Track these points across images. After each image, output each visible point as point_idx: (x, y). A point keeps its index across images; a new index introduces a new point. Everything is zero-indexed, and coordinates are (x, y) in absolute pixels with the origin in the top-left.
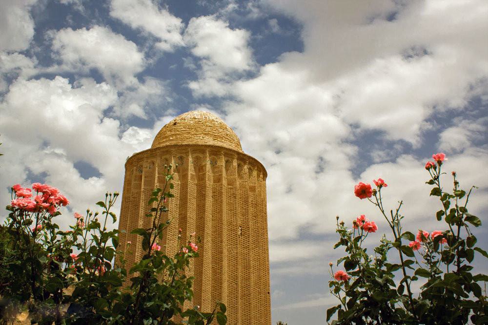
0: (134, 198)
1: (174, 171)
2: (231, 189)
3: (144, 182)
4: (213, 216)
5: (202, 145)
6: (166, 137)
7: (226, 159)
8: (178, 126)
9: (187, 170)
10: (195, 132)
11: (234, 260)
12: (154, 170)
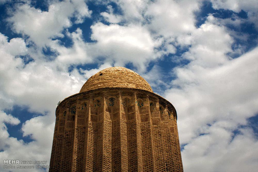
0: (67, 135)
1: (107, 110)
2: (156, 128)
3: (78, 121)
4: (143, 151)
5: (130, 89)
7: (151, 102)
8: (104, 76)
9: (119, 109)
10: (120, 80)
12: (87, 110)
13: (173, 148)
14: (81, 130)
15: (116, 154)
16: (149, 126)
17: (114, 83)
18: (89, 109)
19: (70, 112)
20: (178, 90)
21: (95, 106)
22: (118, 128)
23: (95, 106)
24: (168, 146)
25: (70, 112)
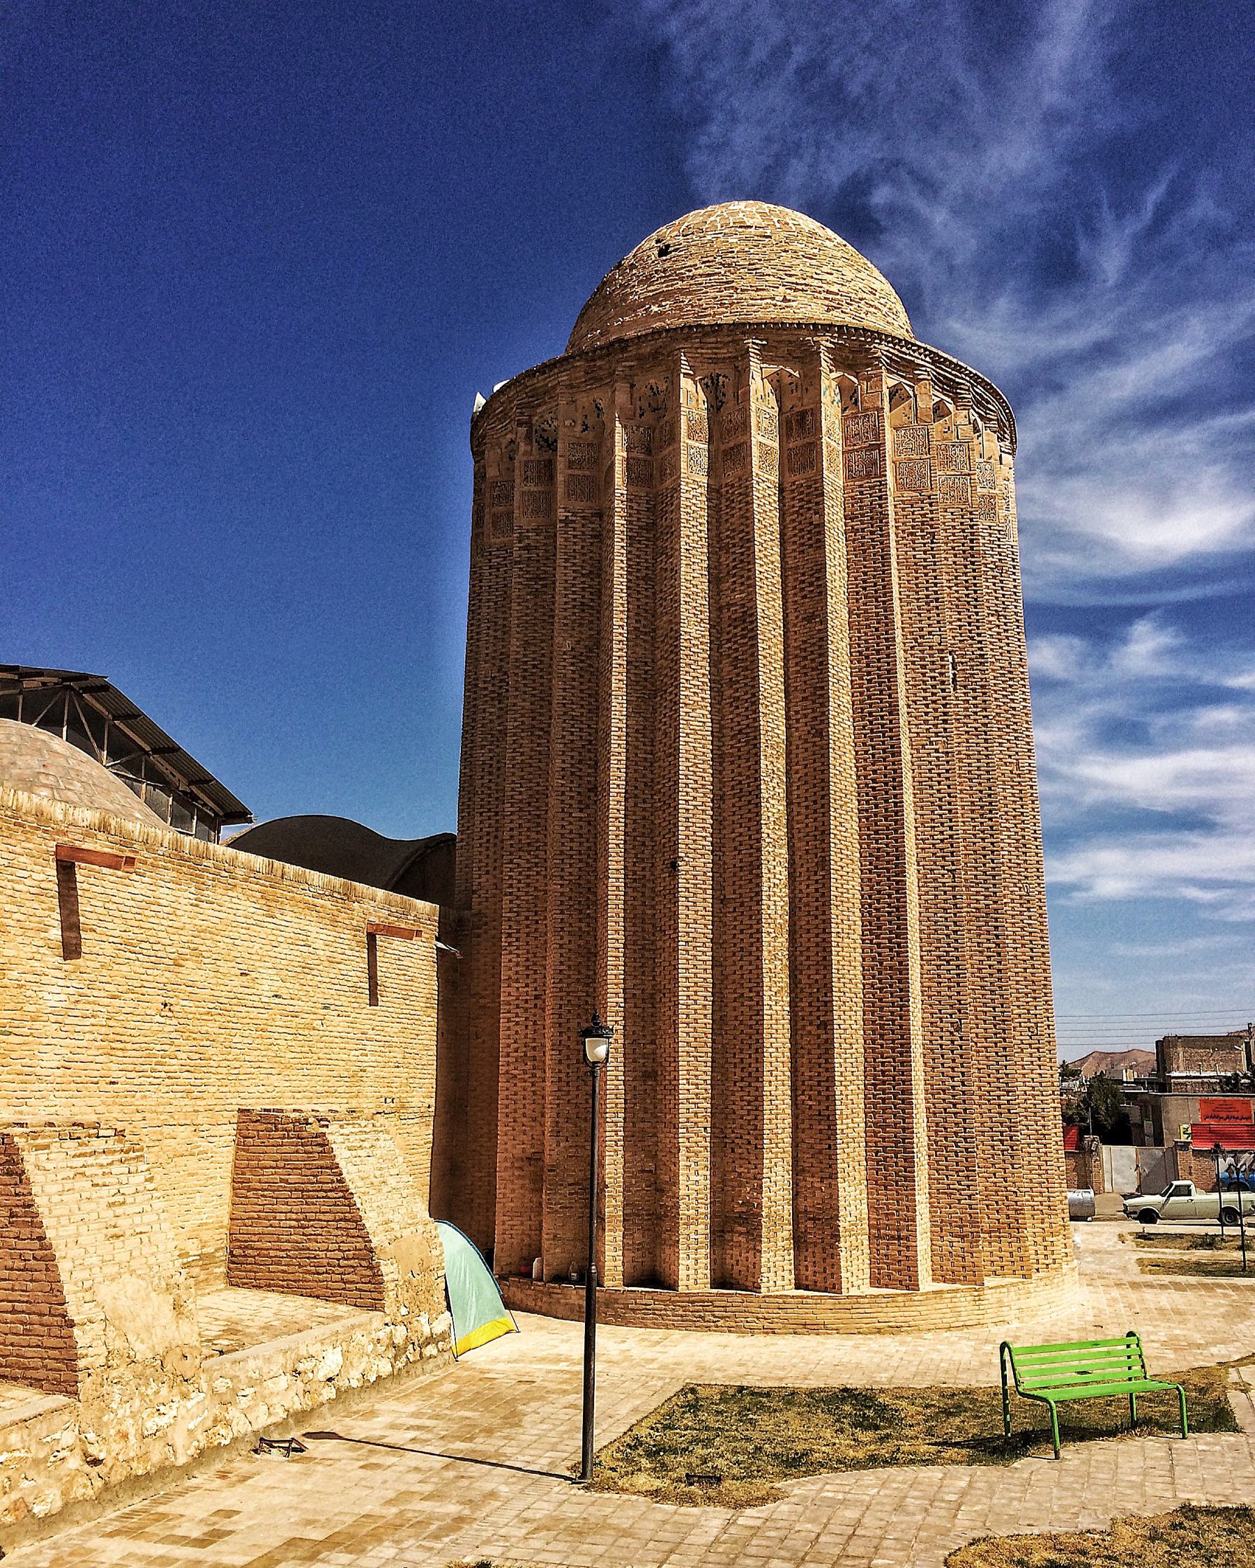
0: (527, 548)
4: (850, 613)
6: (633, 308)
11: (936, 780)
13: (988, 587)
14: (583, 526)
15: (735, 628)
16: (880, 498)
17: (726, 293)
18: (613, 431)
19: (531, 444)
20: (424, 1159)
21: (641, 416)
22: (742, 516)
23: (641, 416)
24: (966, 581)
25: (531, 444)
